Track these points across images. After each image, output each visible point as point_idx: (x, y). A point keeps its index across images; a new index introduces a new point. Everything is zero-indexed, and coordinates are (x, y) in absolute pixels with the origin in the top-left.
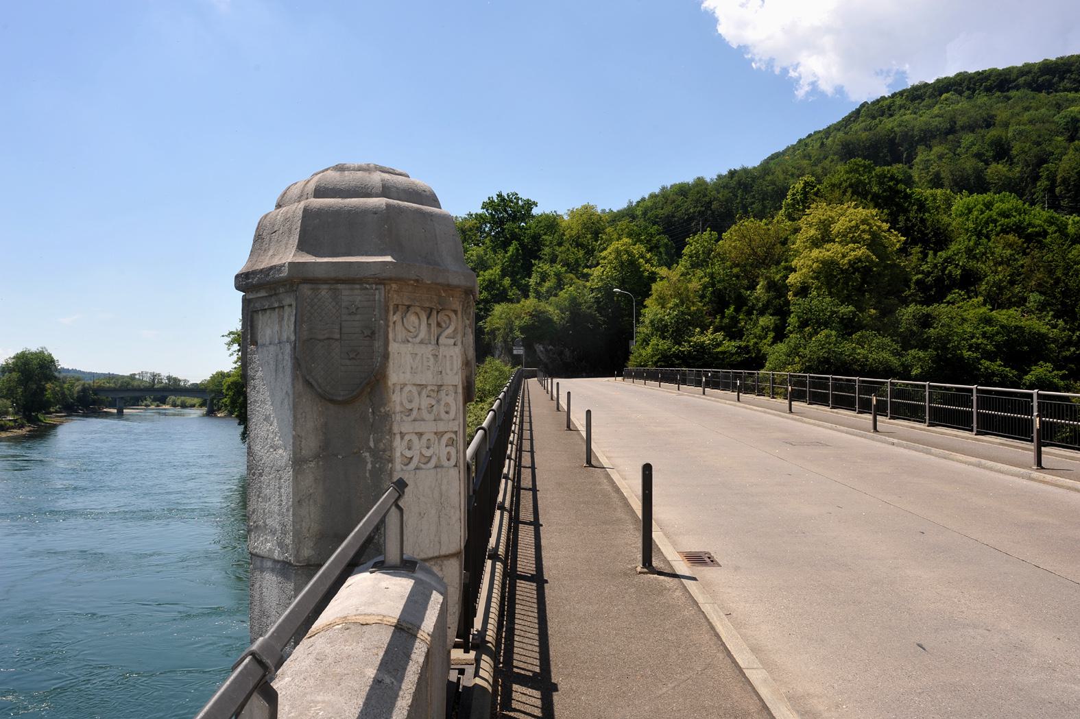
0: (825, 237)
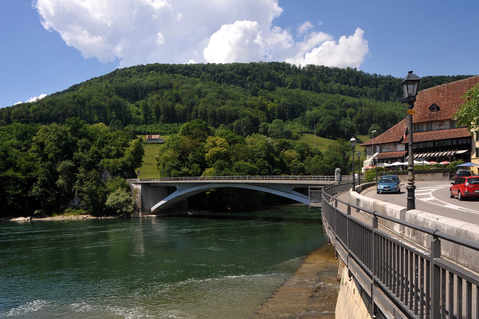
0: (215, 145)
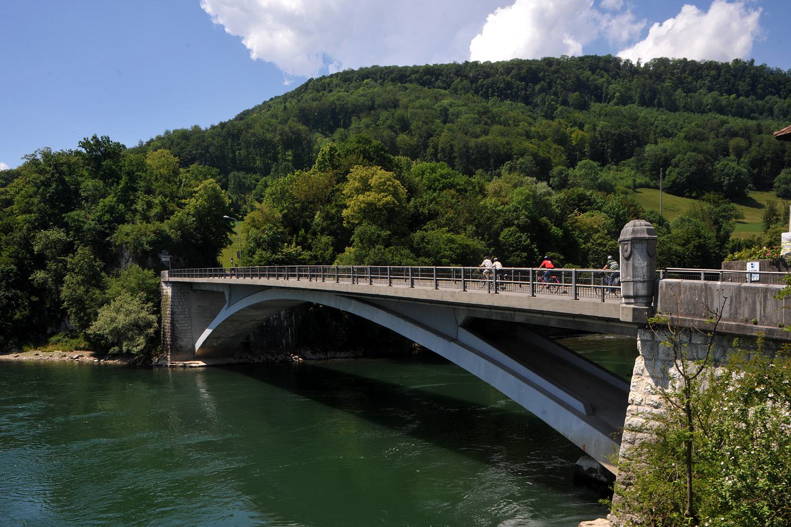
0: (365, 187)
